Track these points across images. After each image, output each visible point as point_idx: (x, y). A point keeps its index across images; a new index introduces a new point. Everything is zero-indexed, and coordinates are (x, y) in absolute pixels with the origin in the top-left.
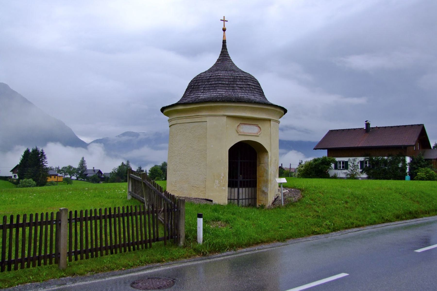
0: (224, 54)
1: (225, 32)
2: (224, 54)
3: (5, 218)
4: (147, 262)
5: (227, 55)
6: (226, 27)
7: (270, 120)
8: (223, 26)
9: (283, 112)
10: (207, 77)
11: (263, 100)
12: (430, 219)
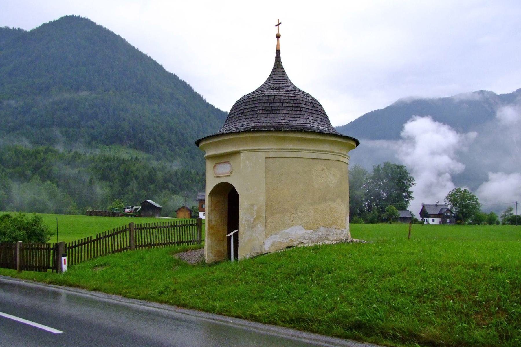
0: (278, 66)
1: (280, 39)
2: (278, 66)
3: (97, 235)
4: (158, 316)
5: (279, 70)
6: (280, 33)
7: (237, 153)
8: (277, 32)
9: (354, 144)
10: (255, 98)
11: (249, 125)
12: (206, 318)
